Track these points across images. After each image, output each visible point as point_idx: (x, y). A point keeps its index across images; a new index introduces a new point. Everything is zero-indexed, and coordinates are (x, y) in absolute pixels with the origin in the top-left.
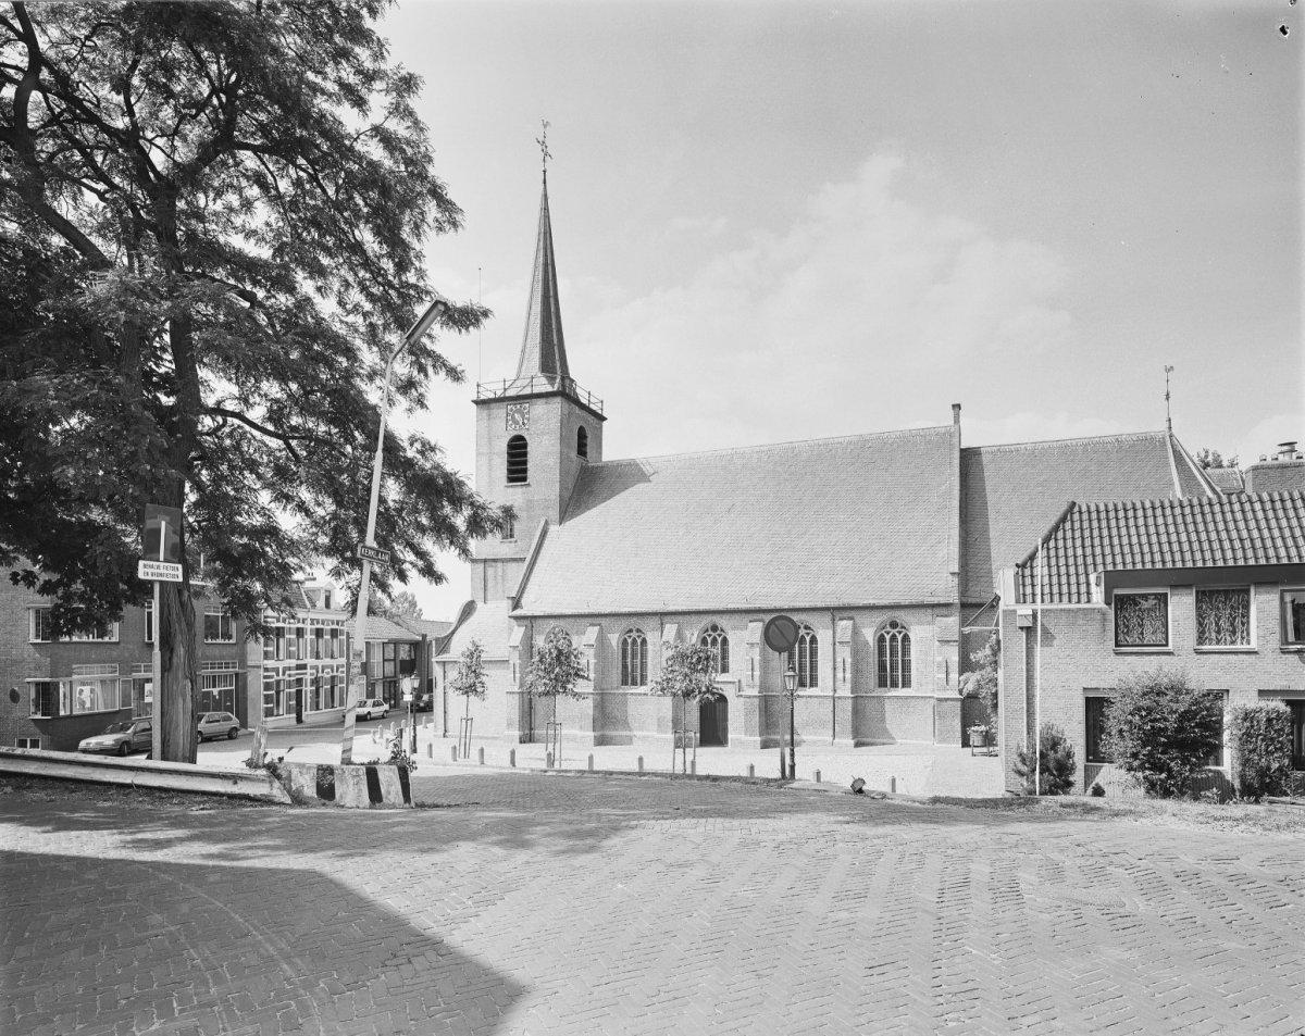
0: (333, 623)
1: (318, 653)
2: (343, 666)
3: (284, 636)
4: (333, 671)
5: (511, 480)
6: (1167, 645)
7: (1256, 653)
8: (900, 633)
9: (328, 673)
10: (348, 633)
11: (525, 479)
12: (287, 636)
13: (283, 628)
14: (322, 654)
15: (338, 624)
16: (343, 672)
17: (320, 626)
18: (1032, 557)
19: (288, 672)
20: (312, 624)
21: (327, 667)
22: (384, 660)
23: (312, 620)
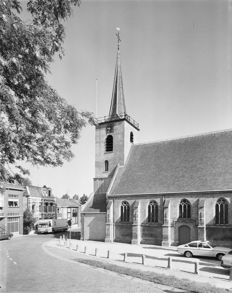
0: (51, 201)
1: (46, 210)
2: (54, 214)
3: (52, 205)
4: (51, 216)
5: (107, 151)
6: (3, 201)
7: (108, 251)
8: (187, 204)
9: (49, 217)
10: (56, 204)
11: (112, 150)
12: (49, 205)
13: (48, 203)
14: (48, 211)
15: (53, 201)
16: (54, 216)
17: (47, 202)
18: (138, 127)
19: (49, 216)
20: (44, 201)
21: (49, 215)
22: (68, 213)
23: (44, 200)
